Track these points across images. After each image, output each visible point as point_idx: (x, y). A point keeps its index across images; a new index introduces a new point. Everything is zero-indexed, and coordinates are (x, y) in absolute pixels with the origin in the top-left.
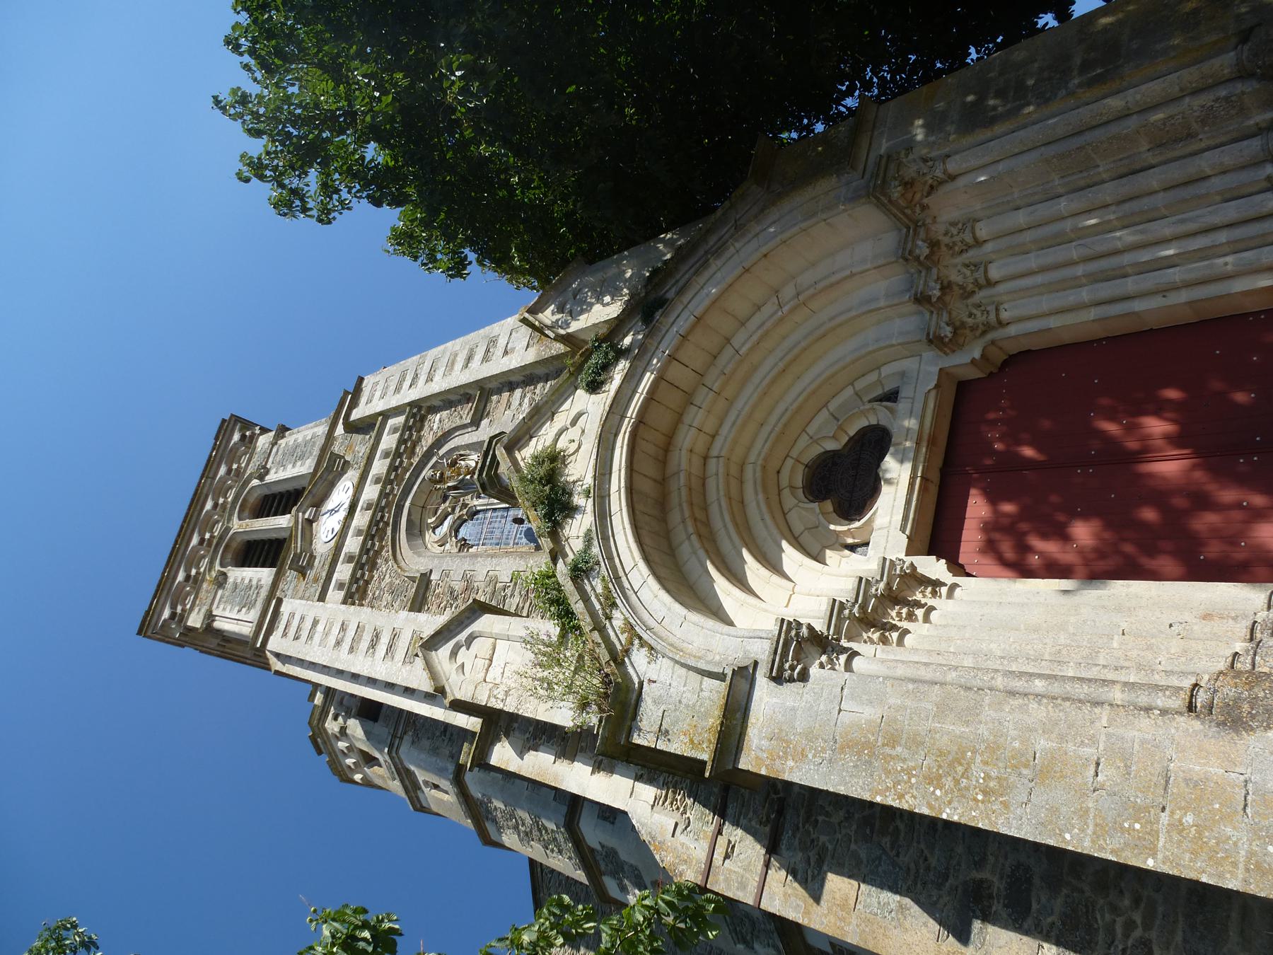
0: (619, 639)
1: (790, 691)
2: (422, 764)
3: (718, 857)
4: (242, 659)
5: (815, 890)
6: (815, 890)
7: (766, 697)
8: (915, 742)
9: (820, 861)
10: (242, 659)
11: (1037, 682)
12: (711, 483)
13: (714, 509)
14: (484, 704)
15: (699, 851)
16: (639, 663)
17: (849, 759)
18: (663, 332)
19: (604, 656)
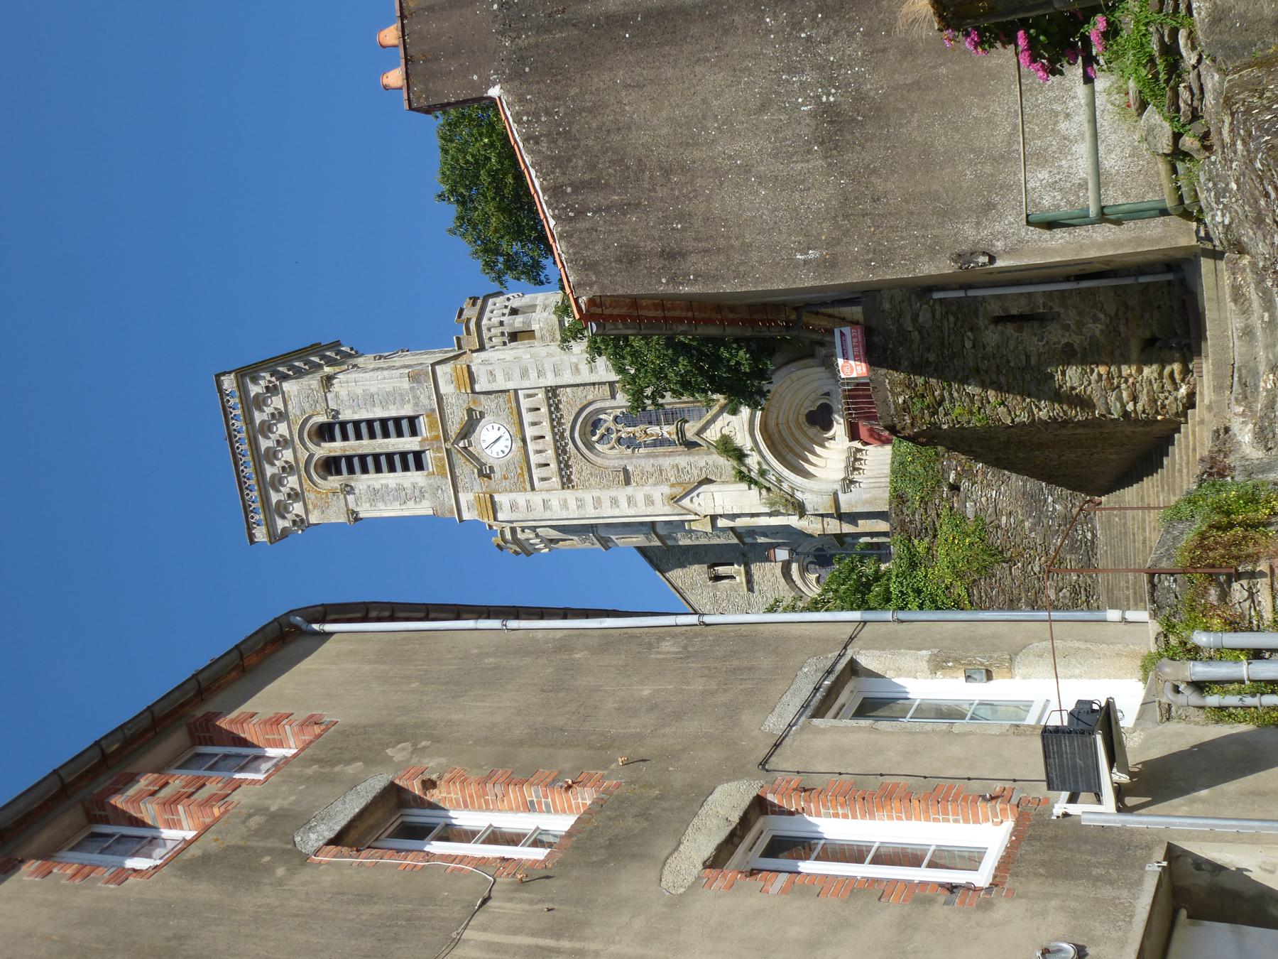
0: (790, 491)
1: (848, 495)
2: (1041, 871)
3: (825, 526)
4: (254, 447)
5: (857, 525)
6: (857, 525)
7: (842, 497)
8: (880, 499)
9: (854, 518)
10: (254, 447)
11: (226, 386)
12: (783, 432)
13: (787, 440)
14: (1121, 725)
15: (820, 526)
16: (799, 495)
17: (867, 505)
18: (1104, 122)
19: (789, 498)
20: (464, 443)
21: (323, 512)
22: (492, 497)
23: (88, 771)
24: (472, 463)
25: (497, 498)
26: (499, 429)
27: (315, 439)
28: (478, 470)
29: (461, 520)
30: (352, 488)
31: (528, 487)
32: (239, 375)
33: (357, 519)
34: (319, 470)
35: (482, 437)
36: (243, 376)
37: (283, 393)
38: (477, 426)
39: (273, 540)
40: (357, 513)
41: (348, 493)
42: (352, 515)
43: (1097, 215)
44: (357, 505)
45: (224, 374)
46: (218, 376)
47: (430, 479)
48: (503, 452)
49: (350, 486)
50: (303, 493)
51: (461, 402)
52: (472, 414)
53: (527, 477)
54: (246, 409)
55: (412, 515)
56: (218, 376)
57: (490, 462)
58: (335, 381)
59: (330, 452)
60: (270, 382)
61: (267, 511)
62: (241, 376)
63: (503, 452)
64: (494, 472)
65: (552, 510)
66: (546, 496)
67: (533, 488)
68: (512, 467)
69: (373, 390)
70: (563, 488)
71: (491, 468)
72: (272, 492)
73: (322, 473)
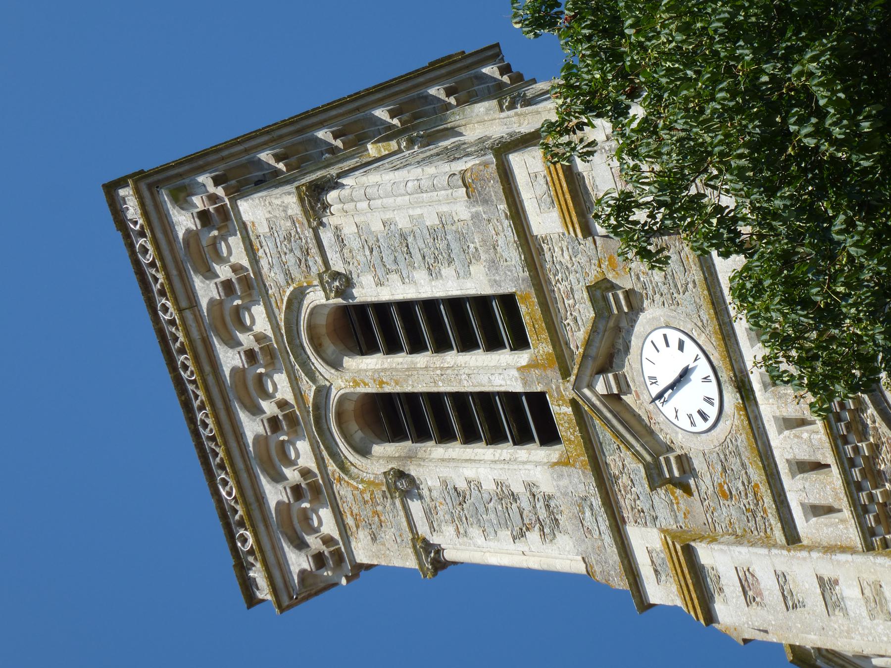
20: (607, 384)
21: (374, 539)
22: (689, 552)
23: (704, 595)
24: (629, 446)
25: (706, 554)
26: (681, 346)
27: (330, 348)
28: (647, 467)
29: (645, 605)
30: (412, 481)
31: (778, 535)
32: (143, 187)
33: (440, 564)
34: (354, 427)
35: (649, 371)
36: (154, 188)
37: (244, 226)
38: (630, 332)
39: (286, 601)
40: (439, 550)
41: (406, 495)
42: (428, 553)
43: (218, 245)
44: (432, 528)
45: (121, 183)
46: (111, 188)
47: (561, 476)
48: (704, 416)
49: (409, 476)
50: (329, 484)
51: (583, 260)
52: (605, 299)
53: (768, 501)
54: (174, 272)
55: (545, 567)
56: (111, 188)
57: (683, 442)
58: (332, 196)
59: (356, 384)
60: (213, 198)
61: (261, 528)
62: (150, 187)
63: (704, 416)
64: (693, 473)
65: (846, 614)
66: (827, 567)
67: (792, 538)
68: (734, 463)
69: (403, 223)
70: (869, 548)
71: (684, 461)
72: (264, 481)
73: (359, 435)
